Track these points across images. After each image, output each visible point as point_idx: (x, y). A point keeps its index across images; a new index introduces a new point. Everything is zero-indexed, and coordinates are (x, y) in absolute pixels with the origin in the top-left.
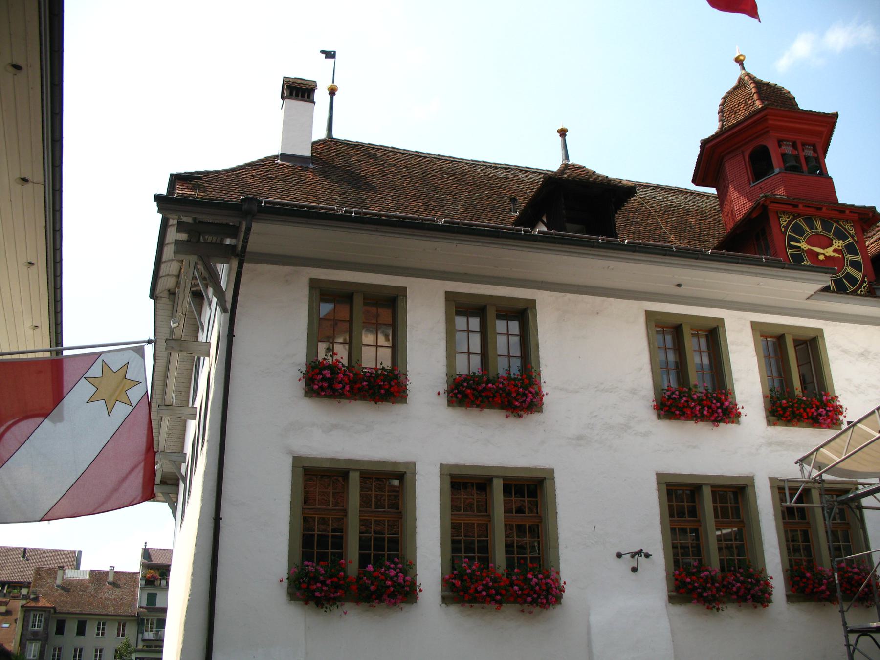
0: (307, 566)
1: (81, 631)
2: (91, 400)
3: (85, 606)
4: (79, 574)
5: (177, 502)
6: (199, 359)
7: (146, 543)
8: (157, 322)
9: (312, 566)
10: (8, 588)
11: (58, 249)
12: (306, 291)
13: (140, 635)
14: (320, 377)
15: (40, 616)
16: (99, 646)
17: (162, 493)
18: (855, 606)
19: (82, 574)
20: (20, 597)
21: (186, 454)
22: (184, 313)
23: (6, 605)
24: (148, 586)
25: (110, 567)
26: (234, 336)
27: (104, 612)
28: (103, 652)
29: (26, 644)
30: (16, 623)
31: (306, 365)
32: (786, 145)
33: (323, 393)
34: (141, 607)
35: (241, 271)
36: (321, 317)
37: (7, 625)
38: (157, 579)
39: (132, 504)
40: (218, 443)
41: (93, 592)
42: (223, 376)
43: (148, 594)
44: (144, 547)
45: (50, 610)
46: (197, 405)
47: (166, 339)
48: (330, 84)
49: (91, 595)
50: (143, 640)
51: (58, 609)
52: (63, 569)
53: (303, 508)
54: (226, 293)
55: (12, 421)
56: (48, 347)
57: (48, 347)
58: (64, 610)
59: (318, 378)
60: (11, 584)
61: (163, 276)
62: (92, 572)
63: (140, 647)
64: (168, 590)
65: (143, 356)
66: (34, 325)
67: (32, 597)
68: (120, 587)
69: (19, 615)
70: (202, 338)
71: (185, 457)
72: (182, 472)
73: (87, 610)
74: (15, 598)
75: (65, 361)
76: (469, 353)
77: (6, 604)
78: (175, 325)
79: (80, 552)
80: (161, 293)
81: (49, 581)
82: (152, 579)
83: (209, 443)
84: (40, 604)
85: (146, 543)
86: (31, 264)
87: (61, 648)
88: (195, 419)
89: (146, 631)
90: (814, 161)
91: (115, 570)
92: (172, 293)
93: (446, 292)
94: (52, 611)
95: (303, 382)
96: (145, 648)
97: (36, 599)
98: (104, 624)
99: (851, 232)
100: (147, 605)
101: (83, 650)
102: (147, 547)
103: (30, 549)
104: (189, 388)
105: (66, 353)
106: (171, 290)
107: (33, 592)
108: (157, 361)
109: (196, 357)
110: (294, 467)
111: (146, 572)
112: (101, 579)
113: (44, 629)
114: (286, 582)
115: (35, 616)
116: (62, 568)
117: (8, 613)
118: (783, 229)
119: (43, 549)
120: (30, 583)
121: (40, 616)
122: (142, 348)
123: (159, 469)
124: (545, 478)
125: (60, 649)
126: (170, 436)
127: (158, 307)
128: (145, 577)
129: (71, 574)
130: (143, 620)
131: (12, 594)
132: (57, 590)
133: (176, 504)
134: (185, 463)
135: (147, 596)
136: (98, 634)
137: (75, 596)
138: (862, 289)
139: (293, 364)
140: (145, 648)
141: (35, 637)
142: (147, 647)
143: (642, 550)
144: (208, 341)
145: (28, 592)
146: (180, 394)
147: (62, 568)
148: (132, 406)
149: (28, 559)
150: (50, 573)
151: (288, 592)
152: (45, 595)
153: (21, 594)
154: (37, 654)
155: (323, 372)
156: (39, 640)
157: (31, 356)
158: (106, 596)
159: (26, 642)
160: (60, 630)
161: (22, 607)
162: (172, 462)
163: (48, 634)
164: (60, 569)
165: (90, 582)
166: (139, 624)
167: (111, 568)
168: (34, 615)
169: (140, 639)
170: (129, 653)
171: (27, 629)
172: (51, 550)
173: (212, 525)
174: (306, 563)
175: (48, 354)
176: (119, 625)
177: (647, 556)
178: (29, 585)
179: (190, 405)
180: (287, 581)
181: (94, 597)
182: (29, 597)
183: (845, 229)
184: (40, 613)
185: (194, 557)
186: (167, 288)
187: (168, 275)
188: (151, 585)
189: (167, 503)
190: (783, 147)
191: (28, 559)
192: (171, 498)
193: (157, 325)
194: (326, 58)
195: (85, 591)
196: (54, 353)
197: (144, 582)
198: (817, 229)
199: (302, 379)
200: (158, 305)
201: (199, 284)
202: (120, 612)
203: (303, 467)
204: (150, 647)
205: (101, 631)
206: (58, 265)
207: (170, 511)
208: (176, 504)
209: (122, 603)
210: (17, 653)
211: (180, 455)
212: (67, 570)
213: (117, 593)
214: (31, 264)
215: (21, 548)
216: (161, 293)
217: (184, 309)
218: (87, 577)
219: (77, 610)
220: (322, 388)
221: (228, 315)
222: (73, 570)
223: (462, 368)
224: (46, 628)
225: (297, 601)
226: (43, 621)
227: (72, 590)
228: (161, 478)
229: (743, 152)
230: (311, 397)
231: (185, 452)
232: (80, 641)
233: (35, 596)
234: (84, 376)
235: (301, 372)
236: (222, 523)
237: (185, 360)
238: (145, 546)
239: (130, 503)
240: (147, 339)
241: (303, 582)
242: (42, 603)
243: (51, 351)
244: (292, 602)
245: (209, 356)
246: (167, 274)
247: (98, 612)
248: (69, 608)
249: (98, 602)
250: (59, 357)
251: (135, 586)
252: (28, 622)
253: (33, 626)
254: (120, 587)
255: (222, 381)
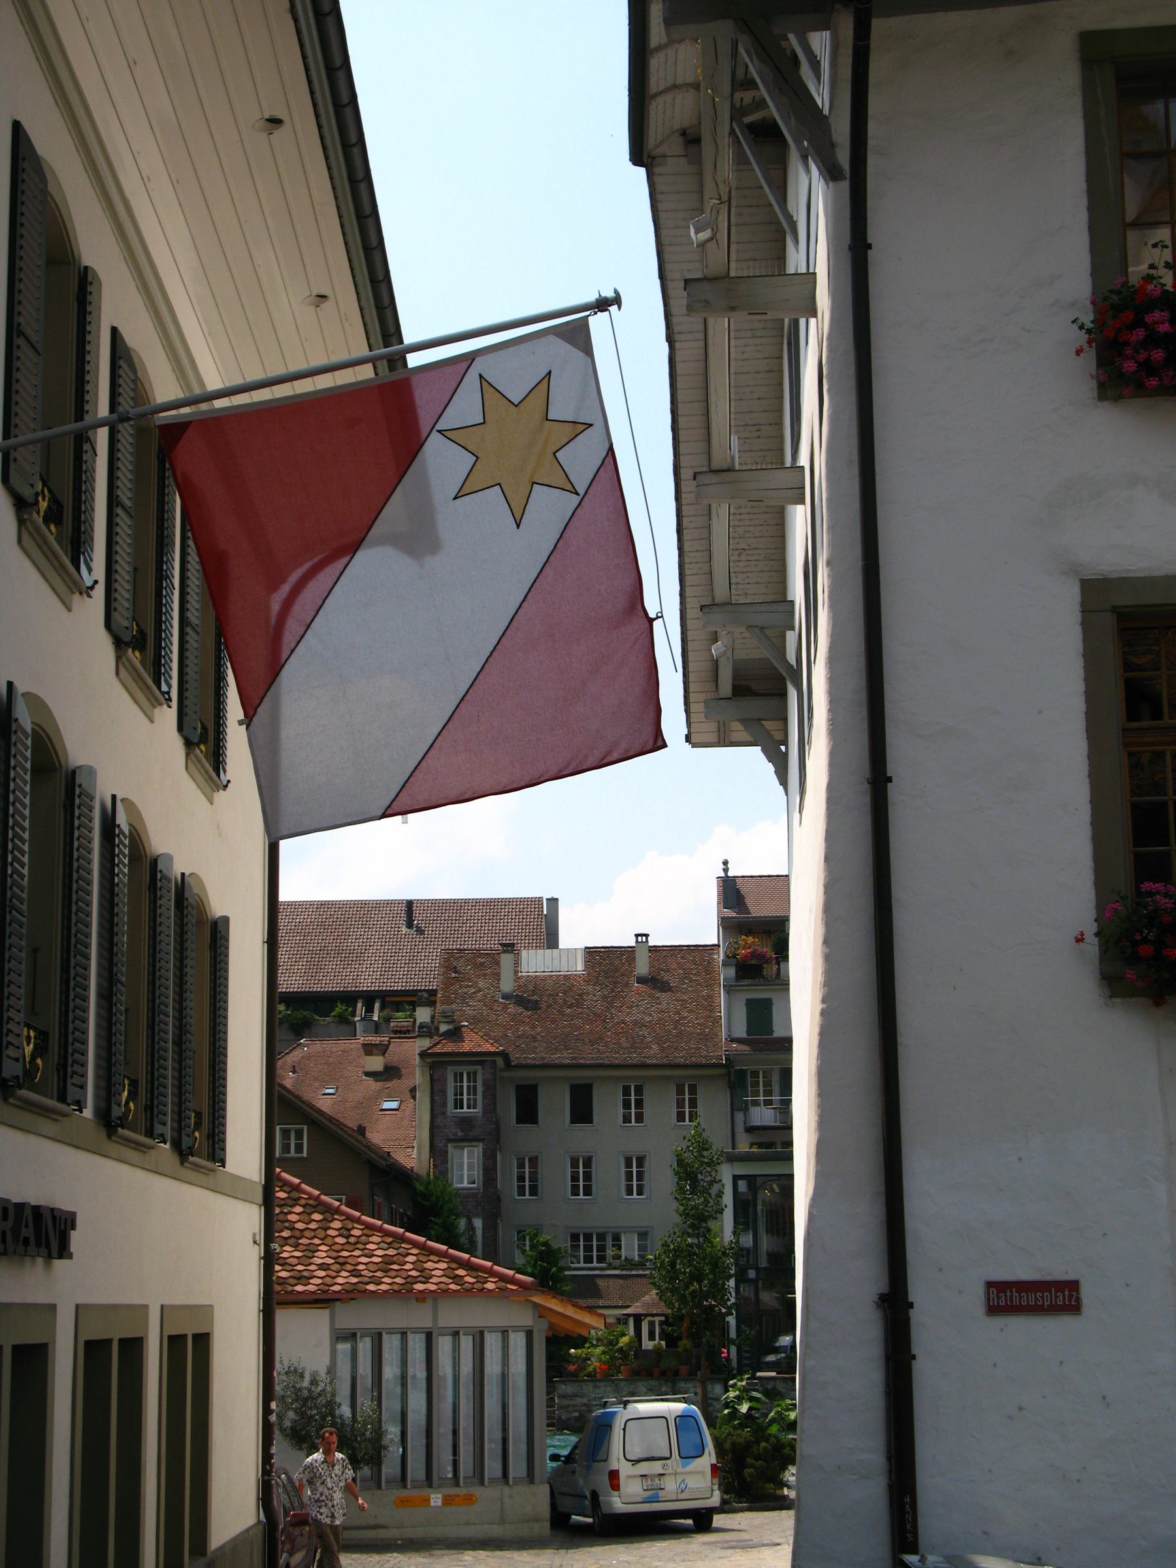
0: (1150, 894)
1: (582, 1113)
2: (466, 490)
3: (585, 1044)
4: (556, 962)
5: (785, 742)
6: (796, 323)
7: (725, 863)
8: (664, 232)
9: (1166, 895)
10: (382, 1008)
11: (340, 68)
12: (1071, 77)
13: (739, 1116)
14: (1140, 333)
15: (472, 1076)
16: (635, 1149)
17: (741, 721)
19: (564, 960)
20: (414, 1031)
21: (792, 603)
22: (725, 198)
23: (384, 1054)
24: (746, 982)
25: (637, 936)
26: (870, 246)
27: (635, 1058)
28: (647, 1164)
29: (447, 1152)
30: (414, 1098)
31: (1093, 303)
33: (1154, 382)
34: (733, 1040)
35: (868, 47)
37: (394, 1105)
38: (768, 961)
39: (605, 761)
40: (859, 564)
41: (599, 1007)
42: (851, 371)
43: (749, 1003)
44: (723, 875)
45: (494, 1061)
46: (804, 461)
47: (687, 281)
49: (595, 1014)
50: (750, 1130)
51: (515, 1057)
52: (512, 952)
53: (1123, 730)
54: (831, 120)
55: (307, 566)
56: (363, 351)
57: (363, 351)
58: (531, 1058)
59: (1133, 338)
60: (388, 999)
61: (661, 93)
62: (593, 954)
63: (743, 1147)
64: (788, 990)
65: (588, 350)
66: (314, 293)
67: (443, 1028)
68: (670, 989)
69: (418, 1077)
70: (795, 261)
71: (792, 613)
72: (788, 658)
73: (589, 1055)
74: (402, 1033)
75: (415, 380)
77: (383, 1049)
78: (704, 235)
79: (553, 902)
80: (662, 143)
81: (481, 984)
82: (754, 962)
83: (831, 570)
84: (467, 1046)
85: (725, 863)
86: (275, 122)
87: (537, 1158)
88: (803, 503)
89: (756, 1103)
91: (651, 944)
92: (691, 139)
94: (500, 1062)
95: (1090, 356)
96: (755, 1150)
97: (455, 1034)
98: (639, 1090)
100: (748, 1032)
101: (594, 1160)
102: (730, 874)
103: (422, 902)
104: (780, 411)
105: (414, 360)
106: (688, 132)
107: (446, 1017)
108: (677, 345)
109: (786, 321)
110: (1088, 610)
111: (737, 943)
112: (617, 970)
113: (485, 1111)
114: (1092, 941)
115: (459, 1077)
116: (509, 948)
117: (390, 1073)
119: (455, 901)
120: (433, 993)
121: (472, 1076)
122: (583, 326)
123: (725, 653)
125: (534, 1161)
126: (743, 558)
127: (659, 188)
128: (734, 956)
129: (535, 962)
130: (742, 1074)
131: (392, 1024)
132: (505, 1007)
133: (783, 748)
134: (793, 629)
135: (744, 1008)
136: (627, 1119)
137: (553, 1021)
139: (1052, 305)
140: (755, 1150)
141: (466, 1132)
142: (760, 1145)
144: (811, 271)
145: (433, 1017)
146: (756, 434)
147: (509, 948)
148: (578, 495)
149: (420, 931)
150: (482, 964)
151: (1101, 973)
152: (475, 1021)
153: (415, 1020)
154: (478, 1174)
155: (1148, 319)
156: (477, 1140)
157: (324, 382)
158: (636, 1015)
159: (447, 1147)
160: (528, 1113)
161: (423, 1055)
162: (757, 631)
163: (497, 1124)
164: (504, 952)
165: (587, 982)
166: (732, 1087)
167: (640, 939)
168: (455, 1074)
169: (740, 1128)
170: (708, 1164)
171: (444, 1113)
172: (434, 902)
173: (867, 799)
174: (1147, 886)
175: (366, 373)
176: (680, 1091)
178: (432, 998)
179: (788, 464)
180: (1096, 940)
181: (604, 1021)
182: (437, 1029)
184: (472, 1068)
185: (826, 893)
186: (677, 126)
187: (675, 87)
188: (753, 978)
189: (759, 748)
191: (420, 931)
192: (767, 731)
193: (665, 240)
195: (579, 1004)
196: (383, 365)
197: (732, 972)
199: (1086, 347)
200: (657, 179)
201: (764, 100)
202: (679, 1057)
203: (1115, 610)
204: (770, 1145)
205: (633, 1110)
206: (348, 112)
207: (770, 768)
208: (783, 748)
209: (681, 1032)
210: (428, 1174)
211: (774, 607)
212: (524, 953)
213: (664, 1006)
214: (275, 122)
215: (400, 902)
216: (662, 143)
217: (721, 185)
218: (580, 966)
219: (565, 1057)
220: (1148, 368)
221: (845, 185)
222: (540, 952)
224: (491, 1107)
225: (1131, 997)
226: (480, 1089)
227: (544, 1006)
228: (734, 679)
230: (1117, 399)
231: (789, 599)
232: (582, 1139)
233: (451, 1027)
234: (438, 427)
235: (1081, 327)
236: (894, 793)
237: (759, 333)
238: (726, 870)
239: (604, 758)
240: (592, 297)
241: (1145, 940)
242: (472, 1043)
243: (372, 360)
244: (1117, 1000)
245: (815, 315)
246: (670, 82)
247: (617, 1058)
248: (540, 1054)
249: (617, 1034)
250: (398, 375)
251: (711, 983)
252: (443, 1092)
253: (459, 1104)
254: (670, 989)
255: (851, 383)
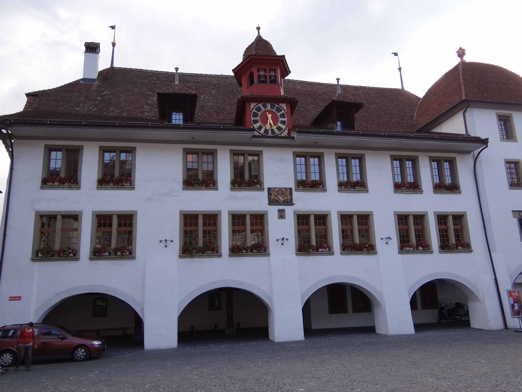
18: (59, 248)
32: (261, 71)
36: (121, 160)
48: (398, 67)
76: (343, 173)
90: (274, 77)
93: (183, 148)
99: (284, 108)
118: (251, 110)
124: (370, 214)
138: (284, 133)
143: (389, 237)
177: (391, 239)
183: (282, 107)
190: (260, 72)
194: (395, 55)
198: (268, 108)
223: (299, 178)
229: (247, 74)
236: (7, 237)
